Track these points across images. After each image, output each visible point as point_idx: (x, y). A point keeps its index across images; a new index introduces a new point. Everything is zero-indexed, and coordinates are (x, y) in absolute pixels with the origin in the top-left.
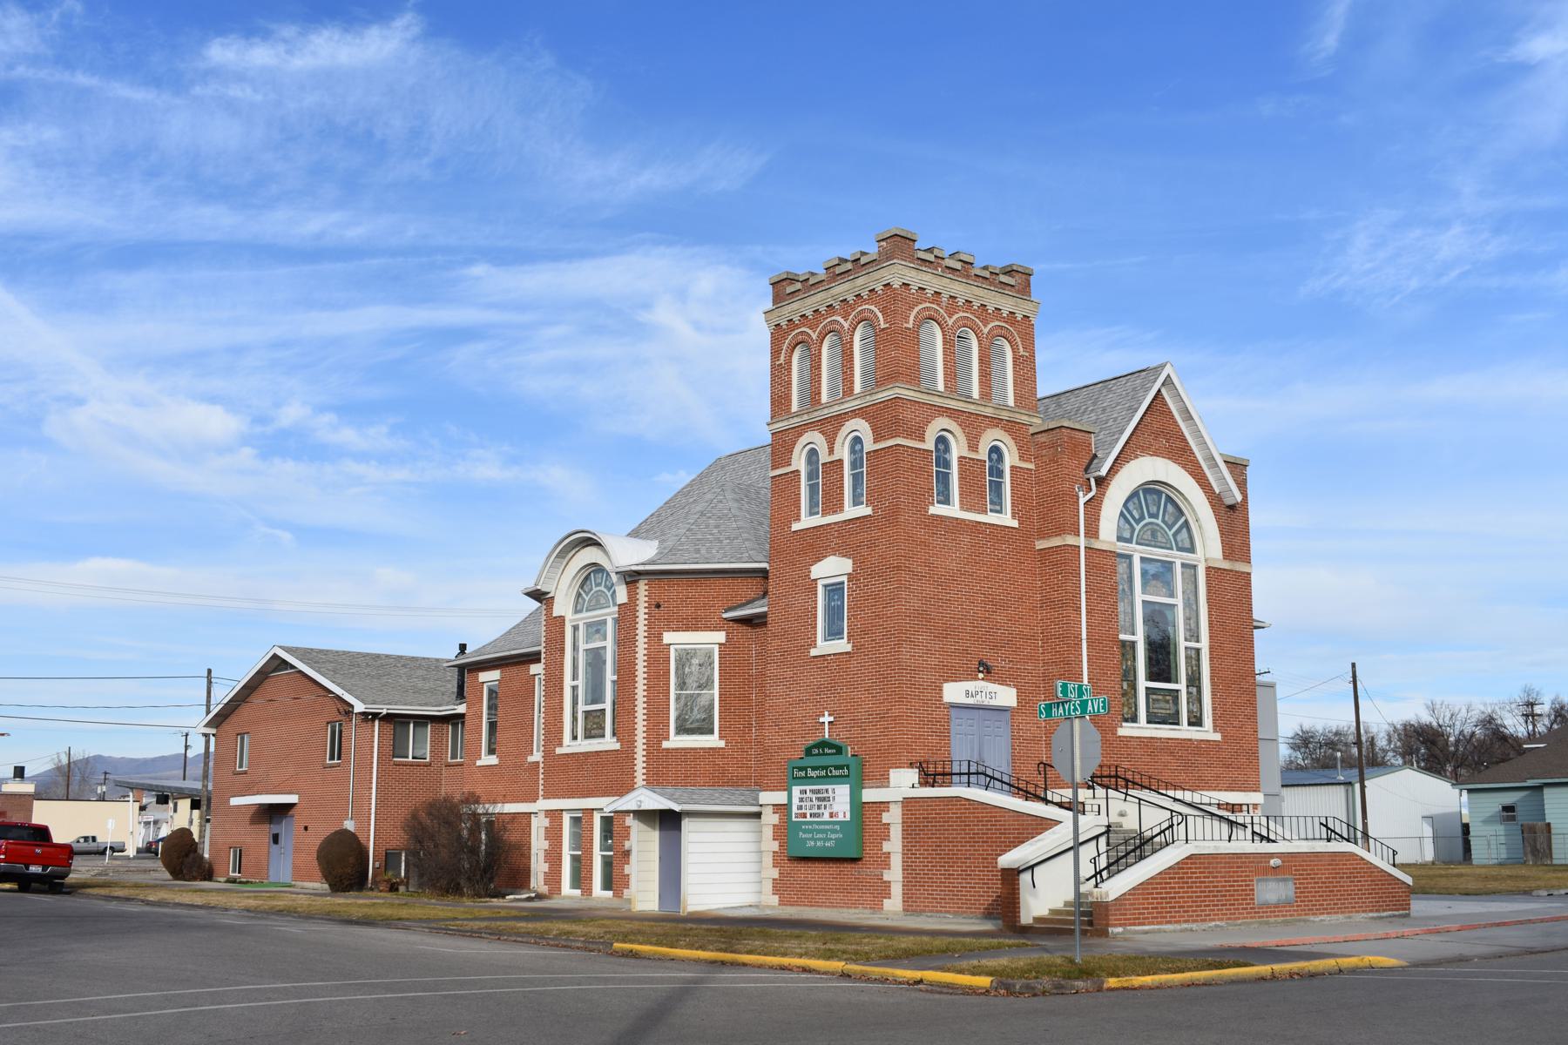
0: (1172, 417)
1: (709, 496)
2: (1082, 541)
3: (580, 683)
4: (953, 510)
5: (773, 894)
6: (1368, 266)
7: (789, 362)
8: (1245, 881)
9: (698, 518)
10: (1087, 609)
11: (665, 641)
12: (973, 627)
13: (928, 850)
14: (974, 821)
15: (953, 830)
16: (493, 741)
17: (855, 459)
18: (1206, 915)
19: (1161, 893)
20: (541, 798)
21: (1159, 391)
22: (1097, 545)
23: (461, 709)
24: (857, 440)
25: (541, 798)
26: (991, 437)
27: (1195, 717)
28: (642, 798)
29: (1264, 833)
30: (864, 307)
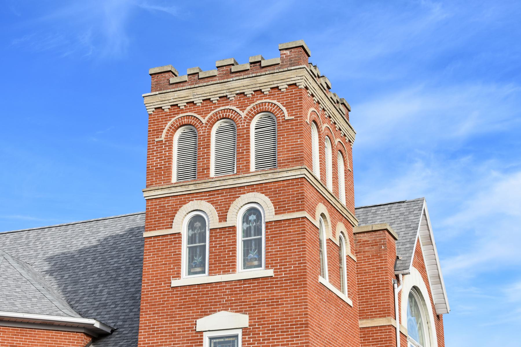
7: (170, 140)
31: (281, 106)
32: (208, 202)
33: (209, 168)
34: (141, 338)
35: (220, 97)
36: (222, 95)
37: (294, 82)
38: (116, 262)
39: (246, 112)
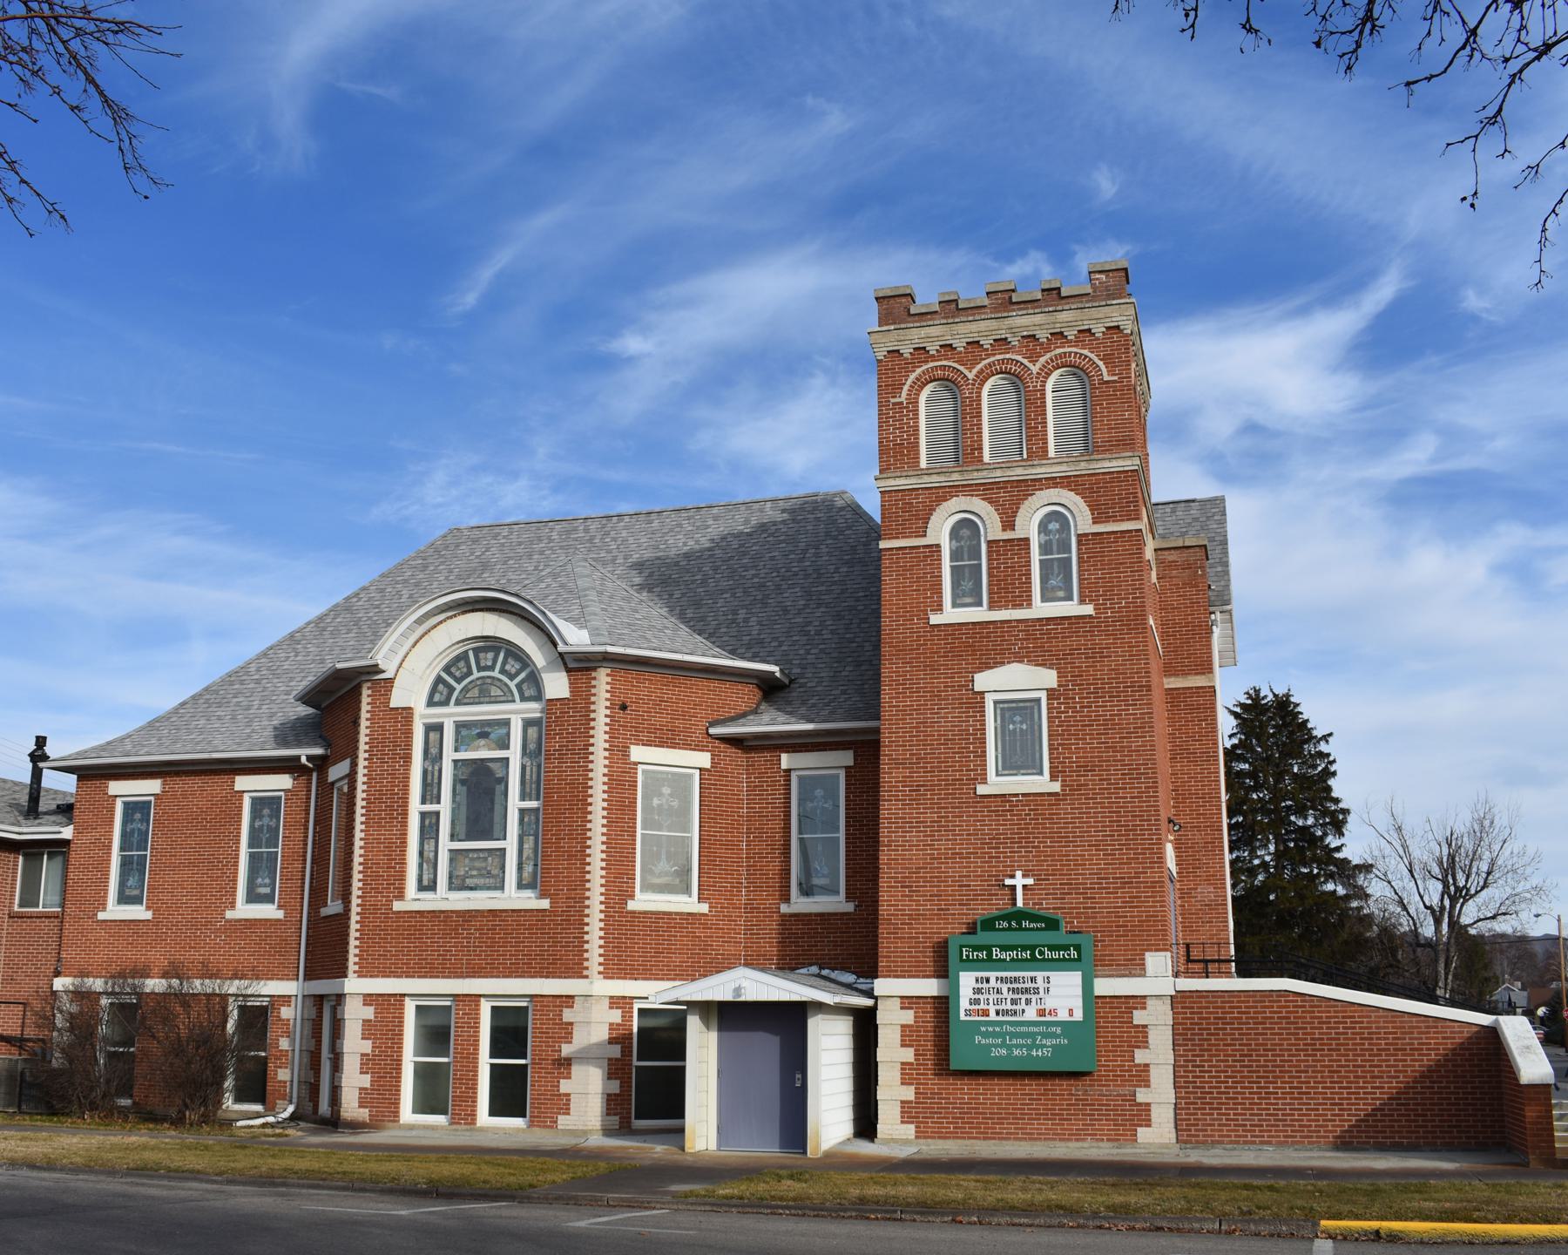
6: (440, 500)
23: (67, 833)
28: (745, 984)
31: (1096, 359)
32: (983, 499)
33: (982, 449)
34: (885, 698)
35: (995, 340)
36: (999, 337)
37: (1116, 324)
38: (754, 576)
39: (1038, 365)
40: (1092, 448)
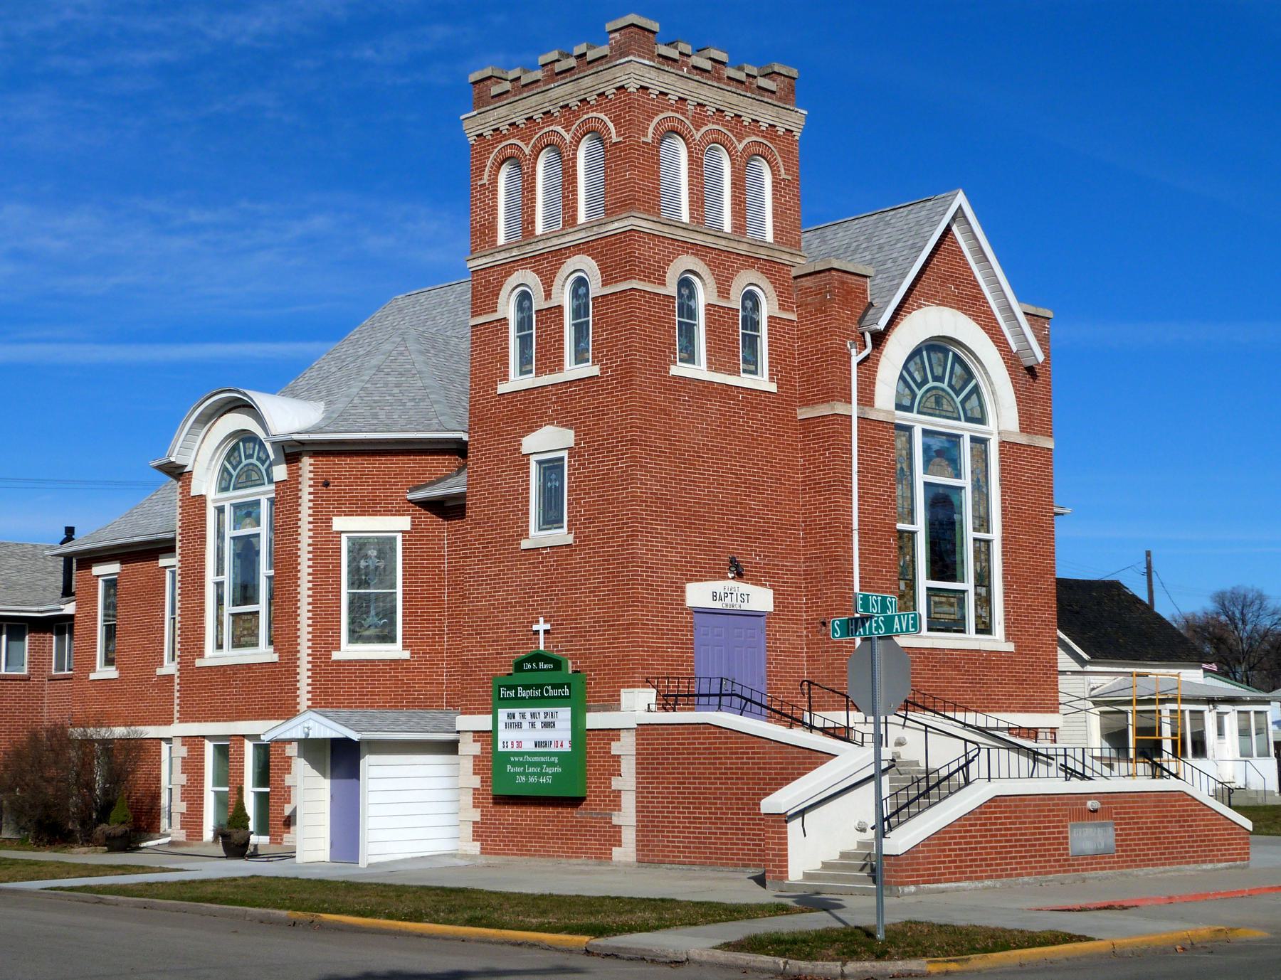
0: (963, 257)
1: (387, 347)
2: (854, 410)
3: (227, 578)
4: (699, 370)
5: (474, 840)
7: (494, 182)
8: (1058, 827)
9: (374, 374)
10: (859, 492)
11: (335, 528)
12: (722, 514)
13: (669, 788)
14: (726, 753)
15: (699, 763)
16: (110, 648)
17: (523, 319)
18: (1012, 869)
19: (960, 843)
20: (176, 721)
21: (948, 229)
22: (873, 415)
23: (69, 609)
24: (581, 283)
25: (176, 721)
26: (744, 280)
27: (984, 623)
28: (311, 724)
29: (1079, 769)
30: (590, 115)
40: (612, 211)
